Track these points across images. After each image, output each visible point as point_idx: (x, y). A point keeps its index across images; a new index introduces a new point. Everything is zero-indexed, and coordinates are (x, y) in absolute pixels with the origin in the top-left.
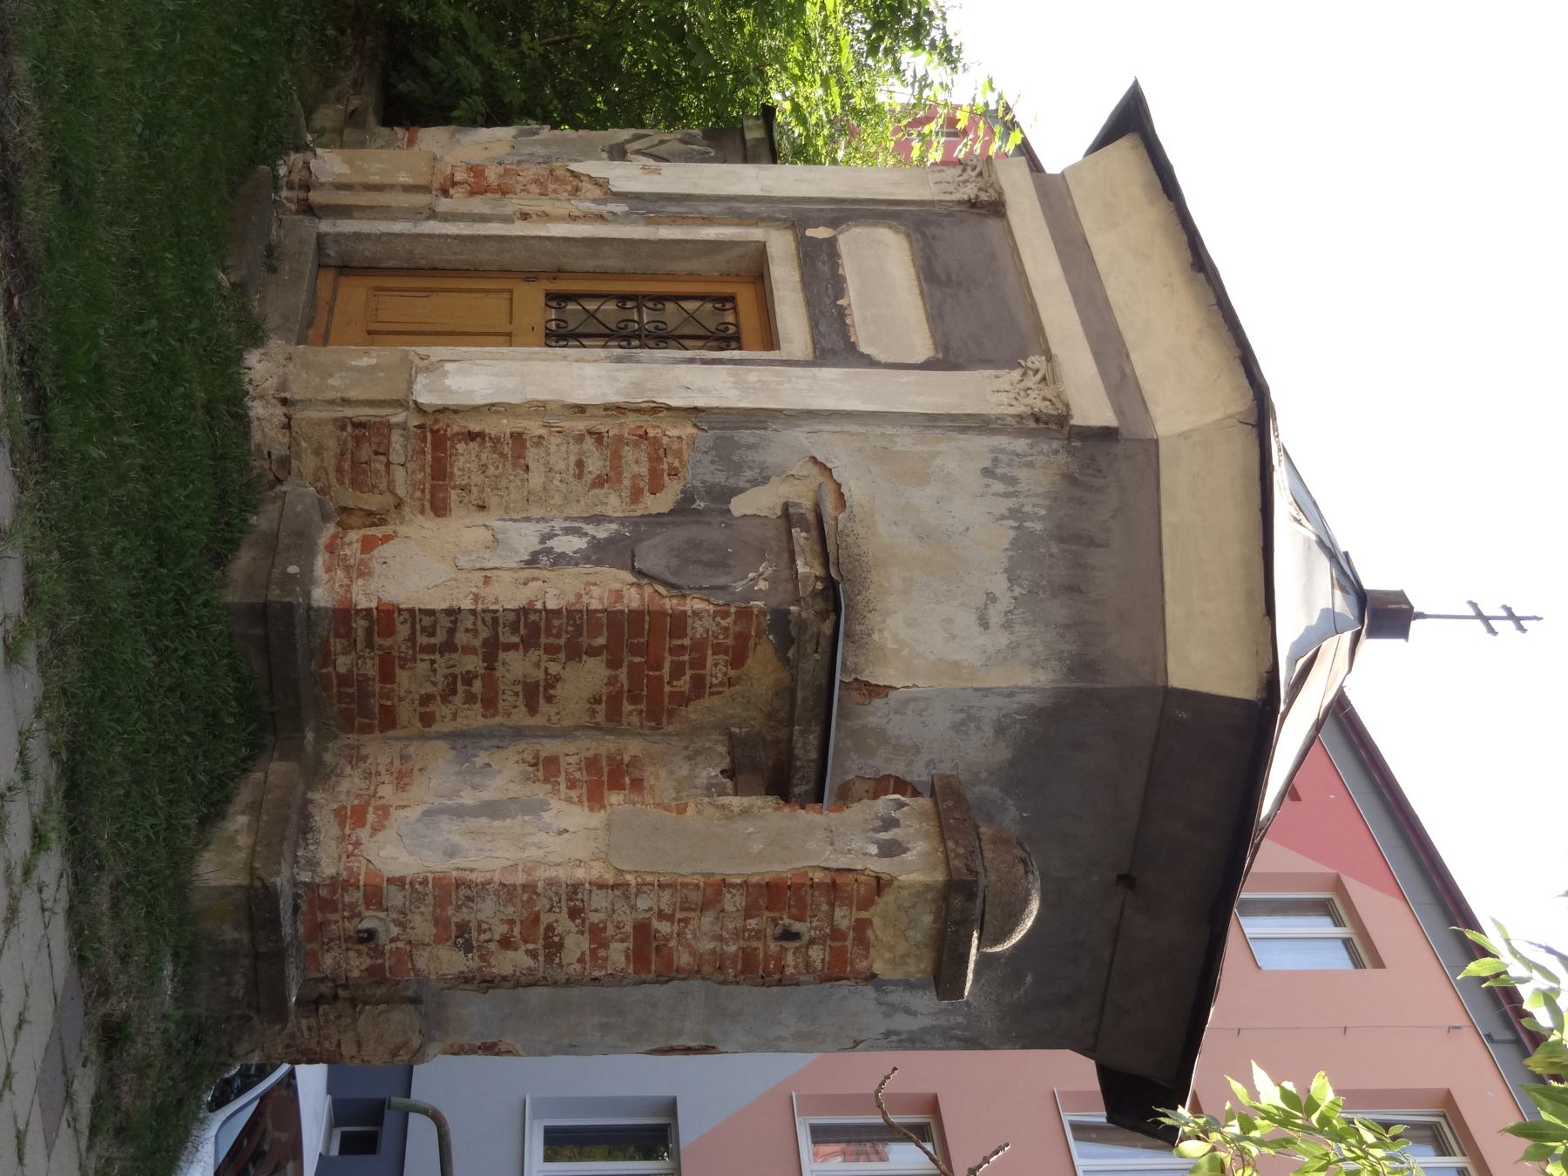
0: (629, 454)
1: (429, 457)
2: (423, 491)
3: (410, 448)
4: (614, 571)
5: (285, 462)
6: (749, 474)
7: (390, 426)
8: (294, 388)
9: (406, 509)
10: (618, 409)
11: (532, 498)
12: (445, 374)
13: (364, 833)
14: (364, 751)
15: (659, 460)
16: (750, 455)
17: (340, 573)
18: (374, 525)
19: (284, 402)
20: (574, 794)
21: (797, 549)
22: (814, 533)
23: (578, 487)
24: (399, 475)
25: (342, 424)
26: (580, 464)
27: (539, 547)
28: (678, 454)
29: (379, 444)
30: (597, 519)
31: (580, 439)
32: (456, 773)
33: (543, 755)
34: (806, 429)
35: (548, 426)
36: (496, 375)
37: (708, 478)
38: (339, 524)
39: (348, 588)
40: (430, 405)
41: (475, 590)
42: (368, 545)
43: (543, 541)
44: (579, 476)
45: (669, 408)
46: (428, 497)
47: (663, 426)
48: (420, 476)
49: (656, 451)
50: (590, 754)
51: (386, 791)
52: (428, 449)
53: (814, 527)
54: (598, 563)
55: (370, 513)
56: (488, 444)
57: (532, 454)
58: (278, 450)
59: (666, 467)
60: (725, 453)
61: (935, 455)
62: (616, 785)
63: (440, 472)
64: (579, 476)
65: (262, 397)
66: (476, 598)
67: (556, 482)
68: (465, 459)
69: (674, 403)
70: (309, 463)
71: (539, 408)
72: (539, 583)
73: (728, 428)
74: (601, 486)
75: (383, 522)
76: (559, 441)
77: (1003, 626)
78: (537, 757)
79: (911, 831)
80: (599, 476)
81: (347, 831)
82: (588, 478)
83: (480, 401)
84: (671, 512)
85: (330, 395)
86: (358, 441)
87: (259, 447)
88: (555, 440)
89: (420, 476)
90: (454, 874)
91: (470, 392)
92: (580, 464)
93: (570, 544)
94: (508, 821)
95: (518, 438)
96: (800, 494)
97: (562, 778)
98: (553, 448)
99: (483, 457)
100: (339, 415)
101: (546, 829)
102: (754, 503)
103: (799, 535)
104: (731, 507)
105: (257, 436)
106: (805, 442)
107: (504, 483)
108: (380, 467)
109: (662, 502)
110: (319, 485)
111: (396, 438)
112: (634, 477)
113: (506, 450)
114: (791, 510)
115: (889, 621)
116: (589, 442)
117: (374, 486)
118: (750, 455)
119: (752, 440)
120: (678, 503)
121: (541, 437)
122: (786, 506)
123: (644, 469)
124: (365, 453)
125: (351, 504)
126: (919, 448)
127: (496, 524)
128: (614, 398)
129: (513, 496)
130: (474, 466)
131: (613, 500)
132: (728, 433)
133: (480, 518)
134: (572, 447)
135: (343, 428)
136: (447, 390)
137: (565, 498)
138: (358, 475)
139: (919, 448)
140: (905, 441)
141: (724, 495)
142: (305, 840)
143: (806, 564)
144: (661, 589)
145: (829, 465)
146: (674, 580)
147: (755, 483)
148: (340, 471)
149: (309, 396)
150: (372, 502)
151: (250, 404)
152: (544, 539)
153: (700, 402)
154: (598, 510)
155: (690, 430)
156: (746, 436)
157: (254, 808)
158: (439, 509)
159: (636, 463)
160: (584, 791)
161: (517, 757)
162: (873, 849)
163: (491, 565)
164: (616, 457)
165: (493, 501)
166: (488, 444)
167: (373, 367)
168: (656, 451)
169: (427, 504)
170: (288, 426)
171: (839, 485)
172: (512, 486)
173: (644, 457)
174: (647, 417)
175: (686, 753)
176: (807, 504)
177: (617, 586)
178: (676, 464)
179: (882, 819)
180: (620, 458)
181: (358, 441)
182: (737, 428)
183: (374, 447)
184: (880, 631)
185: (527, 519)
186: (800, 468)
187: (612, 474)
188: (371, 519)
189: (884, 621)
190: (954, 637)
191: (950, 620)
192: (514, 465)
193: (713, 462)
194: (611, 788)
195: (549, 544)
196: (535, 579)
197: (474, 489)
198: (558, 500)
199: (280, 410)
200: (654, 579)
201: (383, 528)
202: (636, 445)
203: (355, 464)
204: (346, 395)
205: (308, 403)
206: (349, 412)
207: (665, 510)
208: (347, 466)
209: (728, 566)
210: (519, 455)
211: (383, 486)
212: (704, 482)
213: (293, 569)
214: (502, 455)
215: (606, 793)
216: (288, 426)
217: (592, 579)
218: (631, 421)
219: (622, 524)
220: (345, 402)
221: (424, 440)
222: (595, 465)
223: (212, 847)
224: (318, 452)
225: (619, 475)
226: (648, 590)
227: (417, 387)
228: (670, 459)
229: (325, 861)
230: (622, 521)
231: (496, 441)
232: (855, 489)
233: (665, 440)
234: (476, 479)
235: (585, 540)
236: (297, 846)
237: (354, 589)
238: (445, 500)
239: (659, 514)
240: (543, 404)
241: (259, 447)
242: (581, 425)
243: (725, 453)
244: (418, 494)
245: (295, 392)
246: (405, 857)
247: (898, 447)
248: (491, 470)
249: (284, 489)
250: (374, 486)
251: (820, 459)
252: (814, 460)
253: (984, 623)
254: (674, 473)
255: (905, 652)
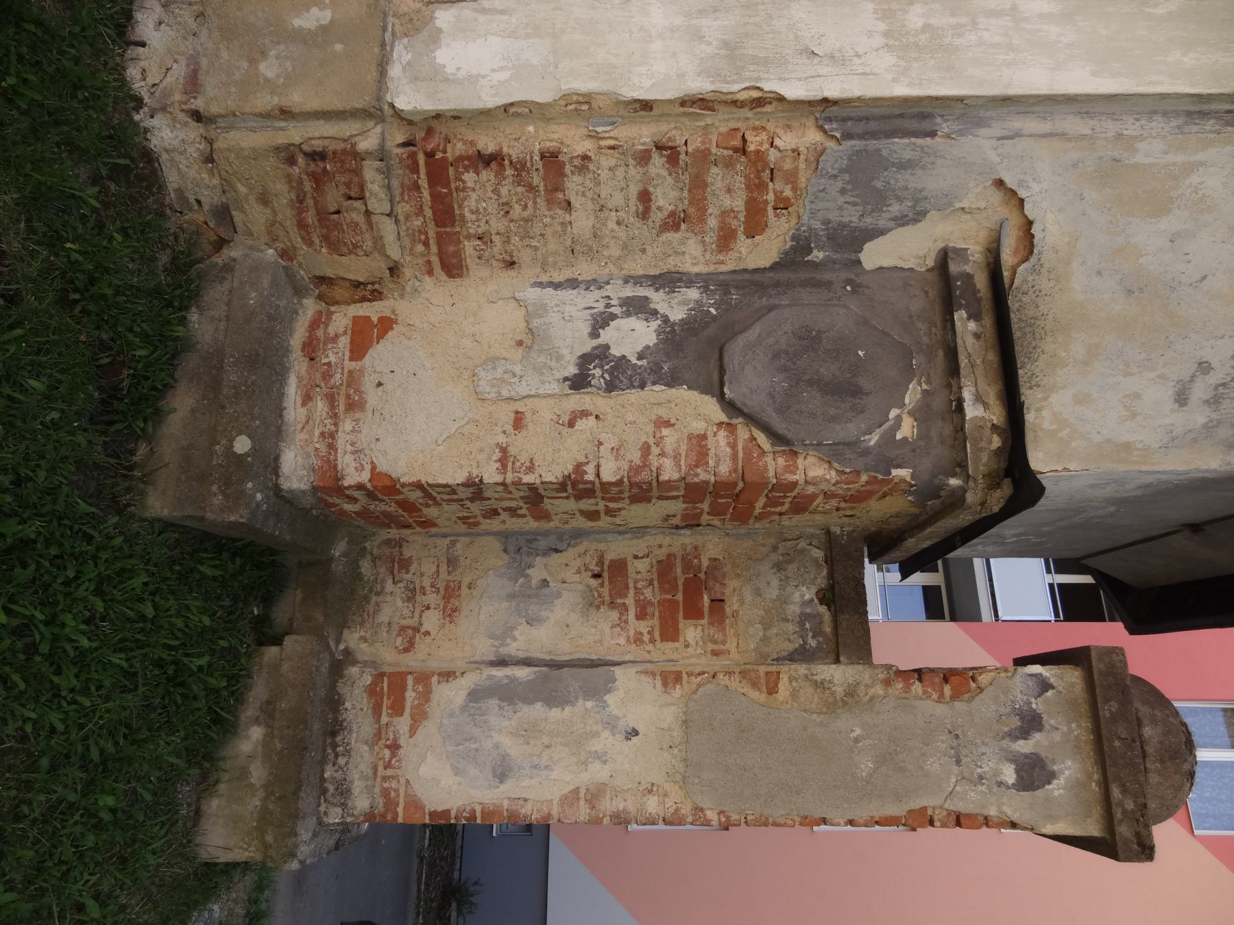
0: (716, 178)
1: (426, 194)
2: (426, 244)
3: (395, 183)
4: (694, 395)
5: (223, 213)
6: (895, 209)
7: (358, 157)
8: (211, 91)
9: (407, 272)
10: (702, 103)
11: (578, 248)
12: (436, 37)
13: (403, 724)
14: (407, 552)
15: (762, 187)
16: (903, 179)
17: (320, 406)
18: (363, 299)
19: (197, 116)
20: (643, 626)
21: (963, 361)
22: (988, 321)
23: (640, 229)
24: (387, 228)
25: (288, 154)
26: (645, 197)
27: (588, 346)
28: (792, 178)
29: (348, 185)
30: (669, 281)
31: (643, 158)
32: (511, 596)
33: (609, 557)
34: (996, 130)
35: (596, 137)
36: (513, 35)
37: (834, 216)
38: (320, 297)
39: (330, 437)
40: (415, 112)
41: (502, 439)
42: (364, 337)
43: (594, 334)
44: (644, 215)
45: (781, 99)
46: (434, 249)
47: (771, 126)
48: (418, 222)
49: (758, 173)
50: (661, 554)
51: (431, 620)
52: (423, 182)
53: (987, 305)
54: (672, 381)
55: (357, 285)
56: (509, 172)
57: (573, 184)
58: (210, 198)
59: (771, 197)
60: (863, 178)
61: (1189, 169)
62: (694, 613)
63: (445, 214)
64: (644, 215)
65: (164, 109)
66: (505, 458)
67: (612, 225)
68: (478, 195)
69: (793, 91)
70: (253, 216)
71: (580, 106)
72: (591, 421)
73: (873, 135)
74: (676, 228)
75: (376, 296)
76: (613, 162)
77: (1207, 402)
78: (601, 562)
79: (1057, 737)
80: (672, 214)
81: (385, 719)
82: (657, 217)
83: (490, 100)
84: (775, 267)
85: (265, 101)
86: (319, 180)
87: (180, 192)
88: (607, 161)
89: (418, 222)
90: (506, 804)
91: (474, 79)
92: (645, 197)
93: (632, 338)
94: (568, 709)
95: (551, 158)
96: (962, 231)
97: (630, 601)
98: (604, 174)
99: (504, 191)
100: (281, 139)
101: (611, 724)
102: (900, 250)
103: (967, 327)
104: (863, 257)
105: (172, 179)
106: (993, 157)
107: (537, 229)
108: (360, 219)
109: (760, 252)
110: (279, 245)
111: (371, 173)
112: (725, 214)
113: (537, 180)
114: (954, 268)
115: (1054, 398)
116: (658, 163)
117: (355, 246)
118: (903, 179)
119: (907, 155)
120: (786, 253)
121: (585, 158)
122: (944, 257)
123: (738, 203)
124: (332, 198)
125: (329, 273)
126: (1171, 158)
127: (532, 294)
128: (699, 85)
129: (552, 246)
130: (492, 207)
131: (693, 247)
132: (873, 144)
133: (506, 281)
134: (632, 171)
135: (291, 161)
136: (437, 76)
137: (625, 247)
138: (330, 230)
139: (1171, 158)
140: (1154, 147)
141: (851, 240)
142: (334, 746)
143: (979, 399)
144: (762, 438)
145: (1022, 193)
146: (780, 427)
147: (902, 221)
148: (302, 225)
149: (232, 105)
150: (356, 268)
151: (149, 123)
152: (601, 322)
153: (833, 90)
154: (671, 263)
155: (814, 136)
156: (901, 147)
157: (268, 712)
158: (453, 268)
159: (727, 193)
160: (656, 622)
161: (578, 563)
162: (1009, 774)
163: (523, 390)
164: (698, 186)
165: (524, 256)
166: (509, 172)
167: (324, 30)
168: (758, 173)
169: (435, 260)
170: (209, 159)
171: (1030, 223)
172: (549, 231)
173: (739, 182)
174: (746, 112)
175: (774, 557)
176: (976, 251)
177: (698, 426)
178: (788, 192)
179: (1021, 714)
180: (705, 185)
181: (319, 180)
182: (891, 134)
183: (343, 189)
184: (1039, 410)
185: (573, 283)
186: (979, 196)
187: (692, 210)
188: (360, 293)
189: (1045, 399)
190: (1134, 415)
191: (1137, 396)
192: (550, 203)
193: (843, 192)
194: (686, 617)
195: (607, 335)
196: (585, 414)
197: (496, 238)
198: (615, 251)
199: (194, 132)
200: (753, 420)
201: (377, 305)
202: (729, 164)
203: (322, 214)
204: (285, 103)
205: (232, 118)
206: (295, 133)
207: (767, 263)
208: (310, 217)
209: (857, 392)
210: (555, 186)
211: (368, 244)
212: (827, 222)
213: (242, 445)
214: (531, 188)
215: (682, 623)
216: (209, 159)
217: (663, 413)
218: (721, 122)
219: (705, 289)
220: (285, 113)
221: (415, 169)
222: (667, 197)
223: (222, 787)
224: (264, 200)
225: (703, 210)
226: (743, 433)
227: (395, 71)
228: (779, 185)
229: (358, 786)
230: (705, 282)
231: (520, 167)
232: (1049, 232)
233: (773, 155)
234: (498, 225)
235: (655, 324)
236: (323, 762)
237: (342, 441)
238: (458, 254)
239: (756, 270)
240: (587, 99)
241: (180, 192)
242: (643, 133)
243: (863, 178)
244: (420, 248)
245: (211, 100)
246: (449, 780)
247: (1139, 158)
248: (517, 211)
249: (234, 254)
250: (355, 246)
251: (1010, 182)
252: (1000, 183)
253: (1182, 399)
254: (783, 205)
255: (1064, 433)
